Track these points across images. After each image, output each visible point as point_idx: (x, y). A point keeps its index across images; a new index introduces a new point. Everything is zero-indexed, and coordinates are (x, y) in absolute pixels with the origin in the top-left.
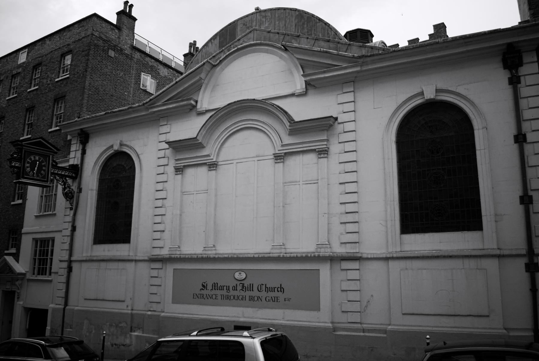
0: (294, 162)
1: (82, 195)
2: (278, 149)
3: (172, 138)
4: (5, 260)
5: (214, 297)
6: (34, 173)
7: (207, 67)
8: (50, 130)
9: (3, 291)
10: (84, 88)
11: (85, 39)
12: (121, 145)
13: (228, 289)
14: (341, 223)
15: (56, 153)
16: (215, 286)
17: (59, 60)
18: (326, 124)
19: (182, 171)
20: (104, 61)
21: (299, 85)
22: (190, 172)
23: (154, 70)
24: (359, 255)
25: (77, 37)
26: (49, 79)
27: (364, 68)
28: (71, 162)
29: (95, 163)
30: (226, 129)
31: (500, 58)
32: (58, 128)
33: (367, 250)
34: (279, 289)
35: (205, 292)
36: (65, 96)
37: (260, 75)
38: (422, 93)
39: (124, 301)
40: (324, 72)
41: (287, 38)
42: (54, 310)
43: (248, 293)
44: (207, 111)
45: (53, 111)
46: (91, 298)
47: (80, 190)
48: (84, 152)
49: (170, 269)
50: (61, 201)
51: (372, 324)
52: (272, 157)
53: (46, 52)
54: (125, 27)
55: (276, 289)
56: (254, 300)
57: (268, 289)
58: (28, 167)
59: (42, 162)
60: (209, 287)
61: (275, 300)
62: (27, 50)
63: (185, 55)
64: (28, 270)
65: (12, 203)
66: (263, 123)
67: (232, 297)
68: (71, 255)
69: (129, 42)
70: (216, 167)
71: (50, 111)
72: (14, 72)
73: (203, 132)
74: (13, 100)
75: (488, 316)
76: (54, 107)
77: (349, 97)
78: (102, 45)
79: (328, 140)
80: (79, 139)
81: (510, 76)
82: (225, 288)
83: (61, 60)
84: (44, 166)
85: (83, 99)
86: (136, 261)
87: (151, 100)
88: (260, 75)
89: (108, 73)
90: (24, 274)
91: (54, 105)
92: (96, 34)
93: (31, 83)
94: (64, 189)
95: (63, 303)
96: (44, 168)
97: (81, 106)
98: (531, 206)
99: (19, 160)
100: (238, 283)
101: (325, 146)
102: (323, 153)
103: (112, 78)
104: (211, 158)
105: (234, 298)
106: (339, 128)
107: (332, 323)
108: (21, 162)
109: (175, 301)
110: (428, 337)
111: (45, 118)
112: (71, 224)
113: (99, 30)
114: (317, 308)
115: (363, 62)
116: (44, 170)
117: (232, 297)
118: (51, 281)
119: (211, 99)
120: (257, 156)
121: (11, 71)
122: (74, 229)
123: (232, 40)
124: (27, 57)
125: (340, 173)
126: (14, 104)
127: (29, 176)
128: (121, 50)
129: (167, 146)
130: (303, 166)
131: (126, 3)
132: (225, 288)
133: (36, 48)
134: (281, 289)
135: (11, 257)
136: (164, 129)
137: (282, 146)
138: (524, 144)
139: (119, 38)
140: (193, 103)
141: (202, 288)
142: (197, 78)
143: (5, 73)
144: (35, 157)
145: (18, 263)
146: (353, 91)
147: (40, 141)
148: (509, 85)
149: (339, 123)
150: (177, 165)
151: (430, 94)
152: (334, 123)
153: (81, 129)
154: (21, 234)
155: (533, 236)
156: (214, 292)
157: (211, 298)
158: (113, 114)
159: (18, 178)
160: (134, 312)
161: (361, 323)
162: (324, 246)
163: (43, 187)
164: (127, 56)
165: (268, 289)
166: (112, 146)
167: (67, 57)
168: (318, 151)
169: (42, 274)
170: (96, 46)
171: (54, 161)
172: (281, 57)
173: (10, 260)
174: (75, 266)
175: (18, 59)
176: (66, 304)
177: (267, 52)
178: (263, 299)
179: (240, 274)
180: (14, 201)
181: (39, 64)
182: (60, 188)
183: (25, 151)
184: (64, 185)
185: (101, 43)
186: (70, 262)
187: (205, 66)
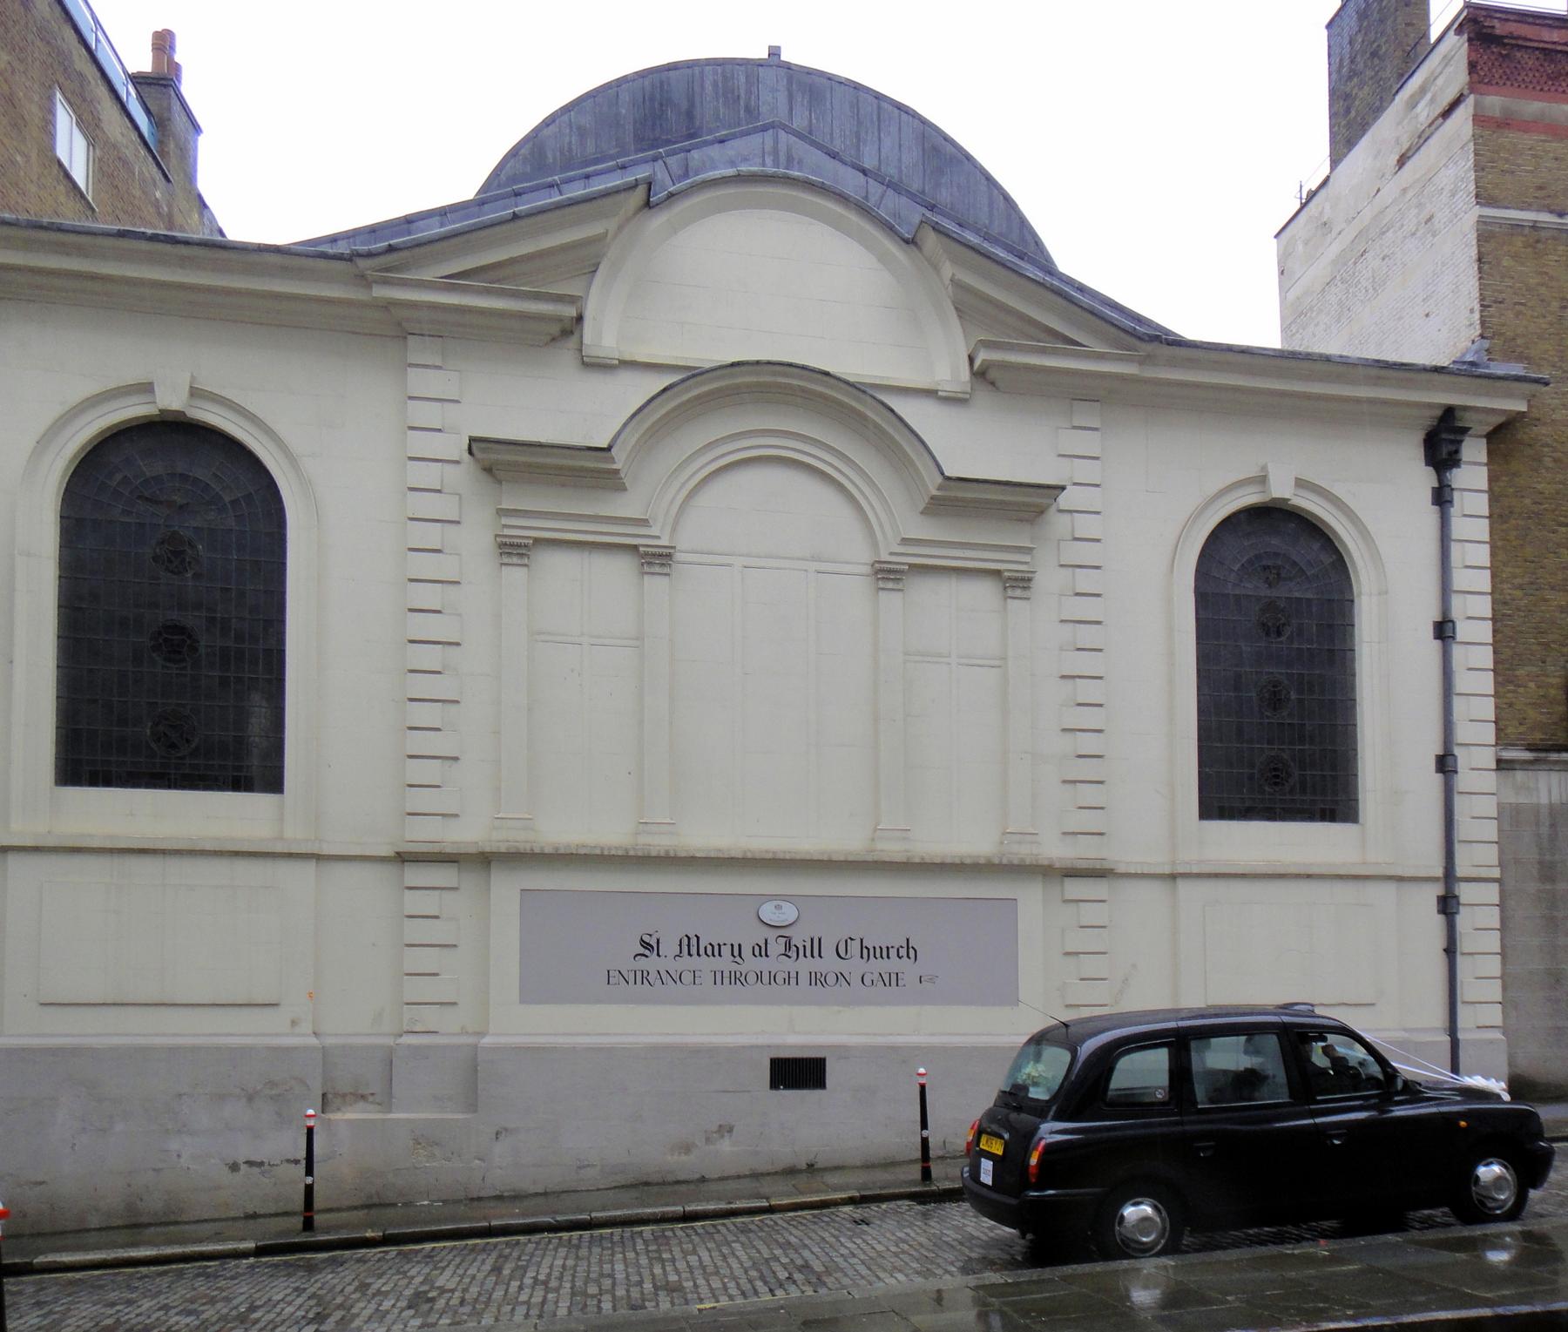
5: (687, 977)
7: (639, 195)
14: (1064, 782)
16: (690, 945)
18: (1027, 503)
21: (949, 371)
22: (559, 567)
30: (709, 446)
31: (1420, 436)
34: (903, 952)
35: (651, 963)
37: (765, 280)
38: (1262, 480)
40: (1043, 351)
43: (805, 966)
49: (506, 889)
52: (867, 569)
55: (893, 952)
56: (824, 983)
57: (866, 952)
60: (669, 947)
67: (752, 978)
73: (632, 437)
81: (1436, 485)
82: (726, 950)
87: (391, 249)
100: (772, 935)
102: (1017, 584)
104: (654, 531)
105: (759, 977)
109: (534, 990)
110: (922, 1070)
115: (1149, 356)
117: (752, 978)
120: (814, 559)
125: (1061, 649)
130: (955, 612)
132: (726, 950)
141: (642, 950)
150: (507, 532)
156: (687, 963)
158: (168, 248)
165: (866, 952)
172: (884, 258)
178: (855, 980)
179: (778, 907)
186: (1449, 876)
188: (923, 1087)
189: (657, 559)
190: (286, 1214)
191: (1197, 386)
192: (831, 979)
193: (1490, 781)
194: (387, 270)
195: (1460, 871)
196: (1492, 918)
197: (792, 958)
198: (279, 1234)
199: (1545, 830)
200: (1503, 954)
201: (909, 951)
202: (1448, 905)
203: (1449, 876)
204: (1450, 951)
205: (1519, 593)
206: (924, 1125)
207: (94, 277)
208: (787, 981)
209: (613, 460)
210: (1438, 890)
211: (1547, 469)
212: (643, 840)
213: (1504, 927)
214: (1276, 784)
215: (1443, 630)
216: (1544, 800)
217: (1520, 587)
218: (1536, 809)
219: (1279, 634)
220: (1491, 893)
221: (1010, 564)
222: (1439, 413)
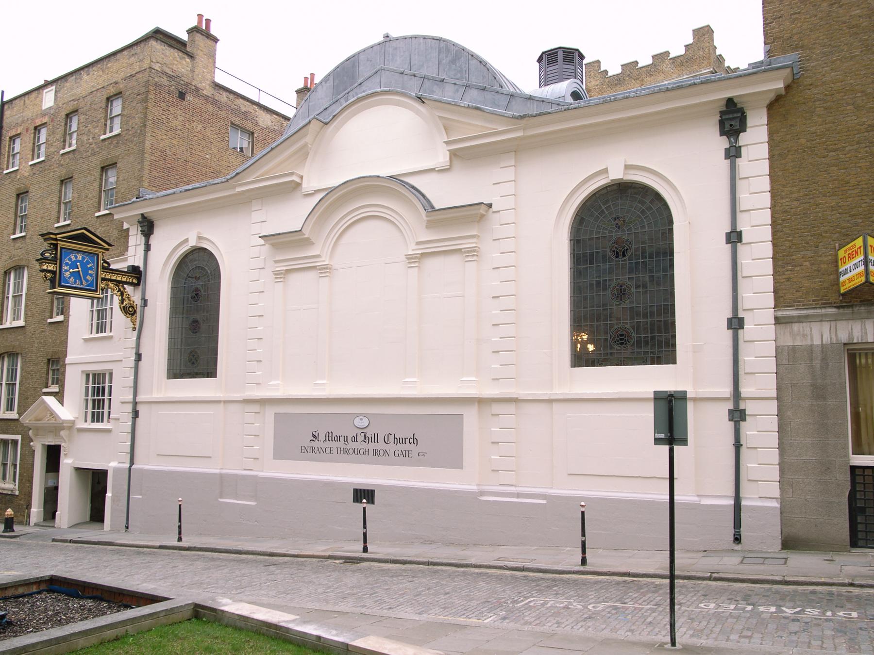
2: (412, 249)
4: (44, 402)
5: (328, 450)
8: (97, 214)
9: (43, 445)
10: (143, 152)
11: (140, 76)
12: (200, 238)
13: (346, 440)
15: (107, 250)
16: (329, 436)
17: (104, 106)
18: (475, 214)
20: (170, 109)
21: (441, 158)
22: (295, 278)
23: (249, 117)
25: (129, 72)
26: (91, 136)
28: (131, 262)
29: (165, 264)
31: (718, 118)
32: (107, 212)
34: (412, 441)
35: (315, 444)
36: (116, 163)
41: (427, 83)
42: (116, 470)
43: (372, 446)
44: (317, 191)
45: (101, 185)
47: (145, 303)
48: (148, 248)
50: (118, 318)
53: (84, 93)
54: (201, 53)
55: (407, 441)
57: (397, 441)
60: (322, 437)
61: (407, 454)
62: (54, 87)
63: (298, 92)
64: (77, 415)
65: (49, 321)
67: (351, 451)
69: (209, 76)
71: (96, 185)
72: (38, 123)
74: (39, 166)
76: (101, 179)
77: (509, 174)
78: (167, 83)
80: (140, 229)
83: (107, 106)
84: (91, 268)
85: (142, 169)
88: (386, 139)
89: (180, 128)
90: (73, 422)
91: (102, 175)
92: (157, 67)
93: (65, 141)
94: (122, 301)
96: (90, 272)
97: (140, 179)
98: (740, 331)
99: (54, 260)
103: (186, 134)
105: (354, 452)
109: (280, 454)
110: (583, 504)
111: (90, 196)
112: (134, 351)
113: (160, 60)
116: (91, 275)
117: (351, 451)
118: (108, 431)
119: (319, 177)
121: (33, 120)
122: (139, 357)
123: (348, 86)
124: (55, 99)
128: (197, 89)
129: (262, 241)
131: (200, 16)
133: (68, 84)
134: (414, 440)
135: (52, 398)
136: (257, 216)
138: (739, 244)
139: (192, 71)
140: (298, 180)
143: (23, 122)
144: (76, 257)
145: (62, 404)
148: (726, 159)
151: (617, 173)
152: (487, 211)
153: (142, 215)
154: (64, 365)
155: (741, 372)
159: (54, 287)
163: (92, 298)
165: (397, 441)
166: (187, 240)
167: (115, 103)
169: (98, 421)
170: (157, 85)
171: (105, 262)
172: (417, 112)
173: (51, 401)
175: (42, 102)
176: (132, 463)
177: (398, 104)
180: (51, 318)
181: (75, 111)
182: (117, 299)
184: (122, 294)
185: (164, 81)
186: (135, 403)
188: (583, 513)
189: (325, 270)
191: (596, 125)
192: (382, 453)
196: (773, 423)
197: (366, 443)
198: (416, 556)
199: (817, 363)
201: (414, 440)
202: (738, 416)
204: (738, 446)
205: (795, 203)
208: (364, 453)
211: (819, 116)
213: (781, 429)
215: (734, 237)
216: (817, 342)
217: (797, 200)
218: (811, 349)
219: (624, 255)
222: (724, 102)
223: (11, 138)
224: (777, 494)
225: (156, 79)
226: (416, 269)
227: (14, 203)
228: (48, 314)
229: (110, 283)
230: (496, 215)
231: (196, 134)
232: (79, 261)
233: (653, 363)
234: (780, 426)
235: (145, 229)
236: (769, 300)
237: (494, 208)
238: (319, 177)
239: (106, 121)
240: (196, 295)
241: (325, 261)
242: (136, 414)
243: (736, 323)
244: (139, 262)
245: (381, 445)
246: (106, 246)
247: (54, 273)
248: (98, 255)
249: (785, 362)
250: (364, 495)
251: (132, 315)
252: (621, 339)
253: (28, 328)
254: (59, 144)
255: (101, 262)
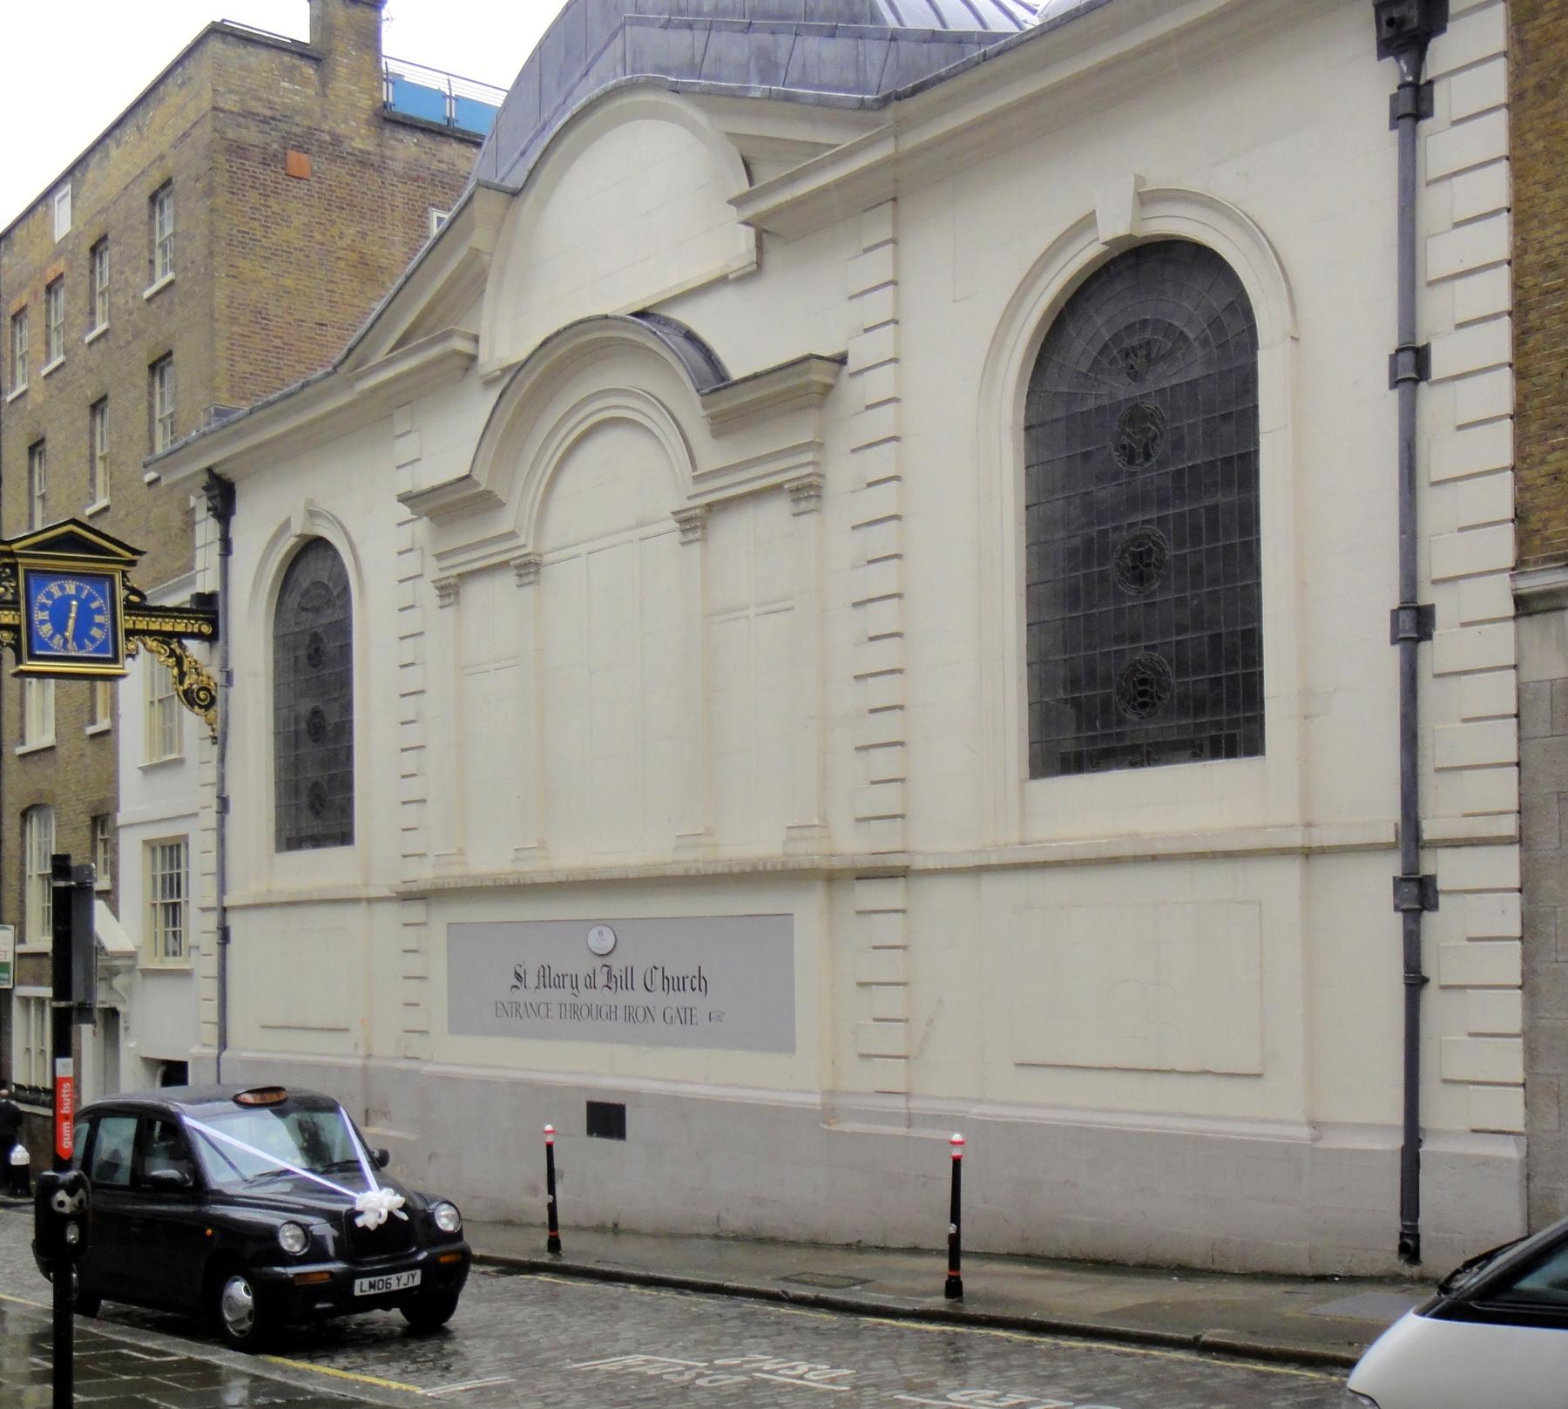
0: (735, 531)
1: (234, 692)
3: (428, 477)
5: (543, 1009)
6: (66, 641)
11: (196, 132)
12: (1146, 198)
15: (132, 563)
16: (547, 979)
17: (146, 218)
19: (457, 594)
20: (271, 201)
22: (476, 592)
24: (898, 861)
27: (911, 141)
33: (933, 842)
34: (696, 982)
35: (522, 996)
39: (346, 1030)
43: (623, 998)
46: (1157, 1077)
47: (229, 677)
51: (1044, 1106)
55: (687, 982)
58: (42, 622)
59: (90, 598)
60: (532, 980)
61: (686, 1016)
66: (627, 408)
68: (222, 889)
70: (537, 572)
75: (1258, 1076)
77: (878, 266)
79: (818, 446)
82: (567, 979)
84: (99, 611)
86: (370, 900)
89: (297, 244)
90: (131, 956)
95: (214, 1040)
96: (98, 619)
100: (599, 962)
101: (809, 470)
102: (807, 492)
104: (521, 541)
105: (590, 1013)
106: (856, 392)
107: (1314, 1125)
108: (17, 610)
109: (460, 1024)
114: (783, 1042)
116: (100, 626)
120: (640, 525)
122: (224, 804)
126: (60, 390)
127: (51, 649)
128: (337, 141)
132: (567, 979)
134: (700, 983)
136: (406, 449)
137: (698, 479)
142: (462, 253)
144: (62, 588)
145: (117, 917)
146: (894, 241)
147: (71, 532)
149: (852, 375)
151: (1117, 222)
152: (837, 375)
153: (209, 470)
154: (116, 829)
157: (537, 1013)
160: (373, 1063)
161: (907, 1094)
162: (806, 832)
164: (363, 161)
166: (1088, 222)
168: (519, 567)
171: (134, 591)
174: (233, 921)
176: (223, 1044)
177: (657, 113)
183: (27, 572)
184: (179, 663)
186: (1411, 836)
187: (476, 204)
190: (915, 1251)
192: (641, 1013)
193: (1501, 641)
194: (357, 367)
195: (1430, 830)
196: (1507, 915)
197: (609, 991)
200: (1527, 985)
201: (700, 983)
202: (1418, 895)
203: (1411, 836)
204: (1415, 982)
206: (955, 1216)
207: (260, 446)
209: (477, 484)
210: (1393, 866)
212: (526, 867)
214: (1143, 705)
219: (1148, 456)
220: (1505, 866)
221: (793, 470)
223: (14, 318)
224: (1515, 1118)
225: (230, 135)
226: (697, 546)
227: (26, 468)
228: (86, 717)
229: (148, 640)
230: (858, 380)
231: (341, 254)
232: (72, 597)
233: (1215, 754)
234: (1528, 922)
235: (217, 502)
236: (1502, 546)
237: (853, 364)
238: (508, 333)
239: (152, 252)
240: (316, 656)
241: (527, 543)
242: (224, 934)
243: (1414, 624)
244: (207, 583)
245: (638, 997)
246: (128, 556)
247: (14, 629)
248: (112, 578)
249: (1542, 728)
250: (606, 1119)
251: (207, 708)
252: (1142, 693)
253: (61, 751)
254: (82, 320)
255: (121, 593)
